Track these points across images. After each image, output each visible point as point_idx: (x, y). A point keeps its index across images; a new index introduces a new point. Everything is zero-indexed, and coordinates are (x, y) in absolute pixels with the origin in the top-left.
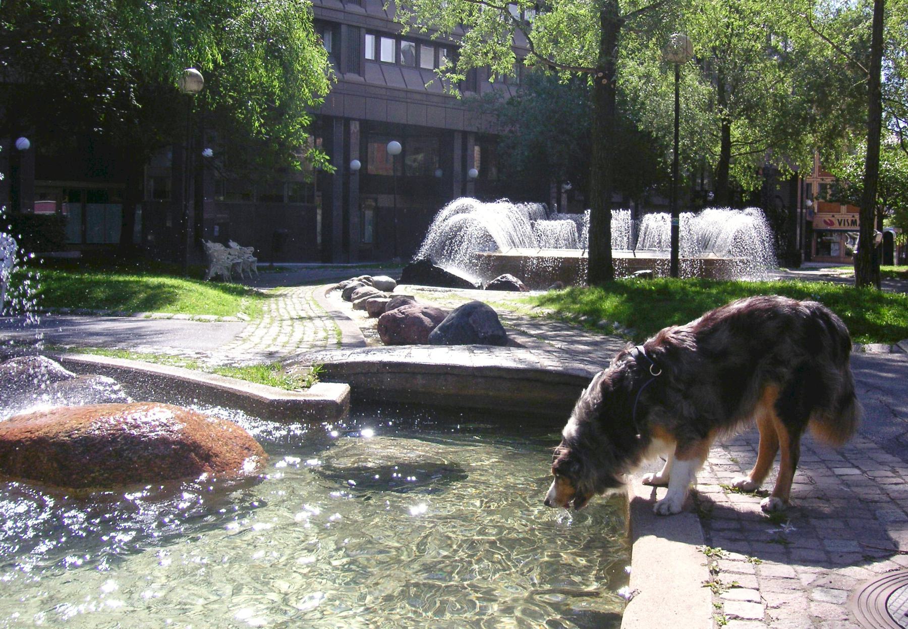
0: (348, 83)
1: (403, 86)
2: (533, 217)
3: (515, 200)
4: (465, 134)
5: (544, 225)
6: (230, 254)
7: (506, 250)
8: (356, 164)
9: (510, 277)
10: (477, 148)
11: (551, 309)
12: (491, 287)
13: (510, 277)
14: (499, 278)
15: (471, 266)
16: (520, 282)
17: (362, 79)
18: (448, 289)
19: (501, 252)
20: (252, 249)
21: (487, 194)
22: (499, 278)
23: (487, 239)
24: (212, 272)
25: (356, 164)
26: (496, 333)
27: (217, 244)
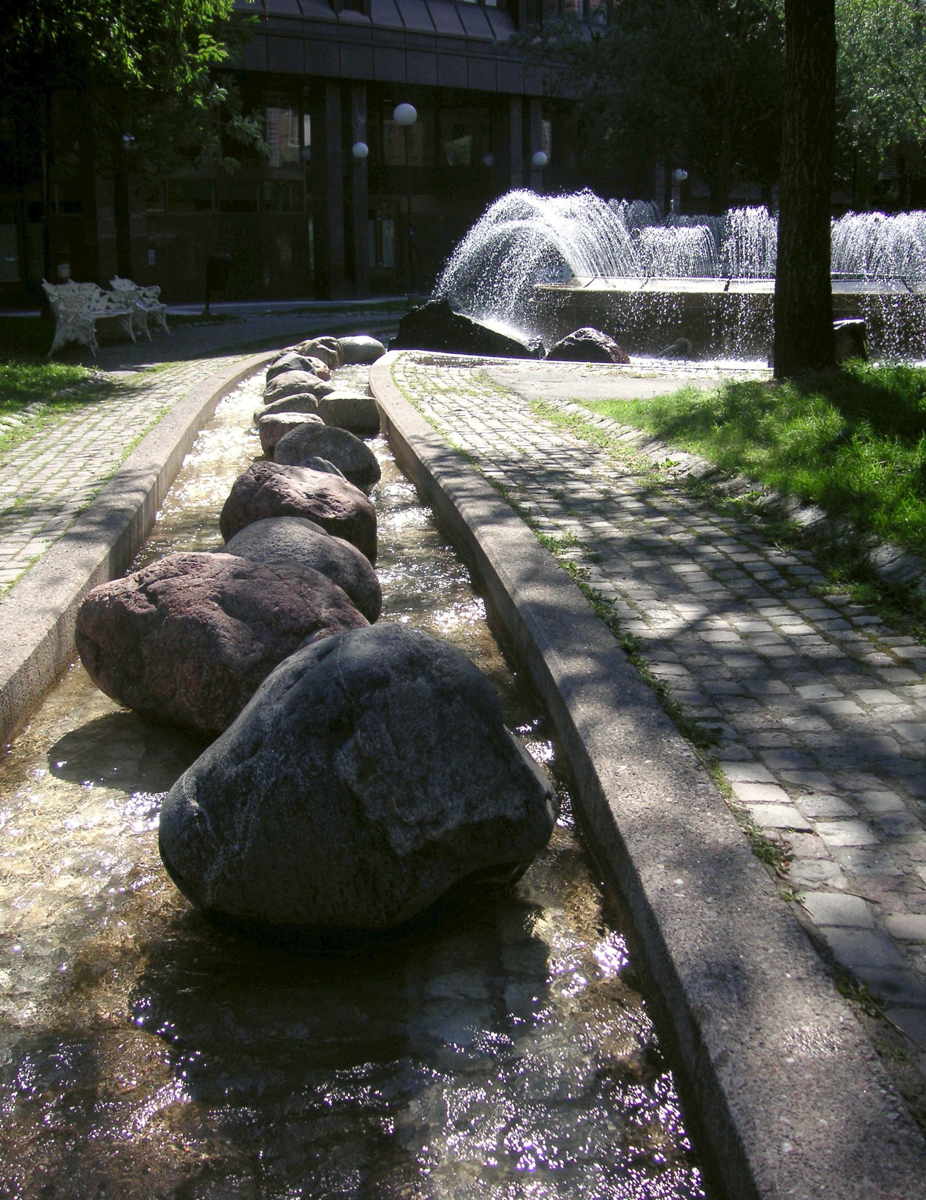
0: (347, 25)
1: (429, 28)
2: (634, 224)
3: (605, 195)
4: (526, 101)
5: (653, 235)
6: (110, 300)
7: (589, 281)
8: (361, 149)
9: (593, 334)
10: (546, 125)
11: (688, 459)
12: (559, 354)
13: (593, 334)
14: (572, 336)
15: (520, 316)
16: (612, 344)
17: (366, 19)
18: (476, 358)
19: (578, 284)
20: (158, 289)
21: (552, 184)
22: (572, 336)
23: (553, 260)
24: (59, 339)
25: (361, 149)
26: (489, 810)
27: (86, 285)
